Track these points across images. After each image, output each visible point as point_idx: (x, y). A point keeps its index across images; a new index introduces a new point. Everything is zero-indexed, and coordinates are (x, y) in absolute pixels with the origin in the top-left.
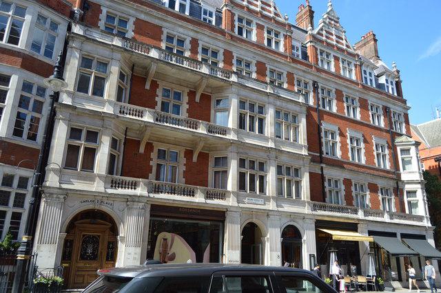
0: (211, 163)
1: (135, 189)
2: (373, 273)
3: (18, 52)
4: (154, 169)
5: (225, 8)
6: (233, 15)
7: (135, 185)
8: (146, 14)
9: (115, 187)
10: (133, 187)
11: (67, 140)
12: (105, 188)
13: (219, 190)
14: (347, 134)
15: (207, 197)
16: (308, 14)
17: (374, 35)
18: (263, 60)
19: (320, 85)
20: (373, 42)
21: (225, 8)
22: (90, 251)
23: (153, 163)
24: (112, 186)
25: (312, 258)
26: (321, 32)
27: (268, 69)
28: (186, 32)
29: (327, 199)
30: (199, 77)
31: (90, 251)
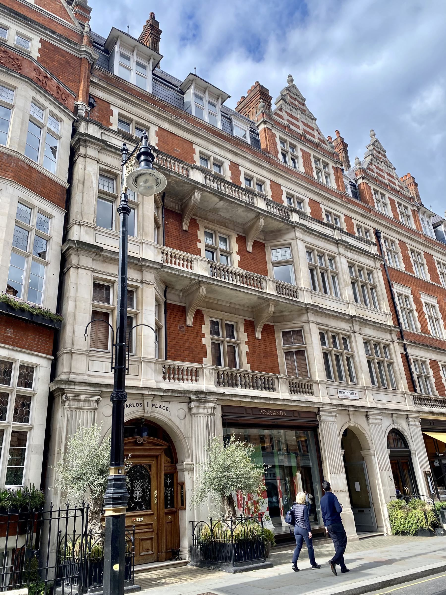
0: (279, 340)
1: (196, 380)
2: (426, 493)
3: (9, 156)
4: (209, 351)
5: (262, 126)
6: (274, 136)
7: (196, 375)
8: (171, 122)
9: (169, 379)
10: (194, 378)
11: (92, 302)
12: (157, 382)
13: (303, 380)
14: (421, 299)
15: (291, 391)
16: (342, 147)
17: (413, 178)
18: (316, 198)
19: (382, 234)
20: (413, 187)
21: (262, 126)
22: (138, 493)
23: (207, 341)
24: (164, 378)
25: (429, 478)
26: (370, 167)
27: (323, 211)
28: (223, 153)
29: (418, 389)
30: (252, 215)
31: (138, 493)
